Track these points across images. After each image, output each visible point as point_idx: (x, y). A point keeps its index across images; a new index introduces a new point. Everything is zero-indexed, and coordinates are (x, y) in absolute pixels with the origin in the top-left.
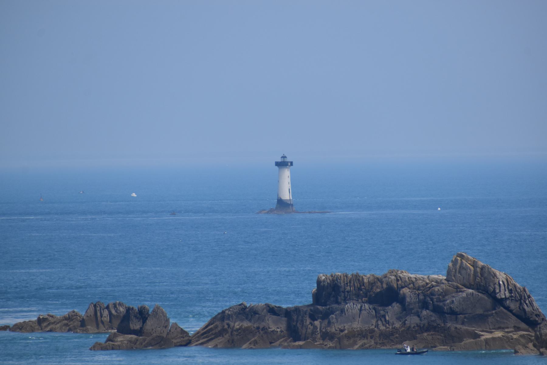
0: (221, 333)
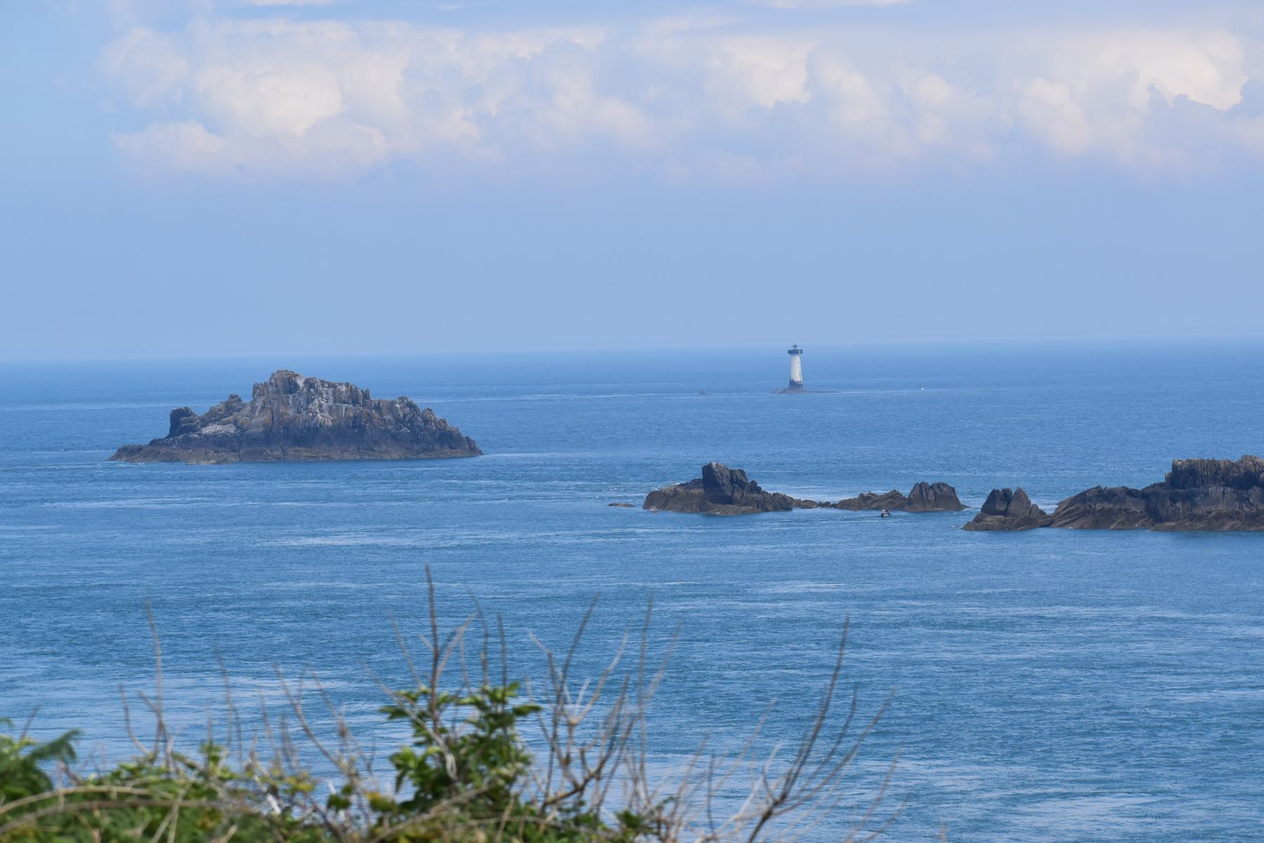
0: (1081, 516)
